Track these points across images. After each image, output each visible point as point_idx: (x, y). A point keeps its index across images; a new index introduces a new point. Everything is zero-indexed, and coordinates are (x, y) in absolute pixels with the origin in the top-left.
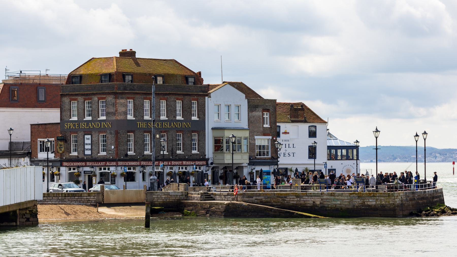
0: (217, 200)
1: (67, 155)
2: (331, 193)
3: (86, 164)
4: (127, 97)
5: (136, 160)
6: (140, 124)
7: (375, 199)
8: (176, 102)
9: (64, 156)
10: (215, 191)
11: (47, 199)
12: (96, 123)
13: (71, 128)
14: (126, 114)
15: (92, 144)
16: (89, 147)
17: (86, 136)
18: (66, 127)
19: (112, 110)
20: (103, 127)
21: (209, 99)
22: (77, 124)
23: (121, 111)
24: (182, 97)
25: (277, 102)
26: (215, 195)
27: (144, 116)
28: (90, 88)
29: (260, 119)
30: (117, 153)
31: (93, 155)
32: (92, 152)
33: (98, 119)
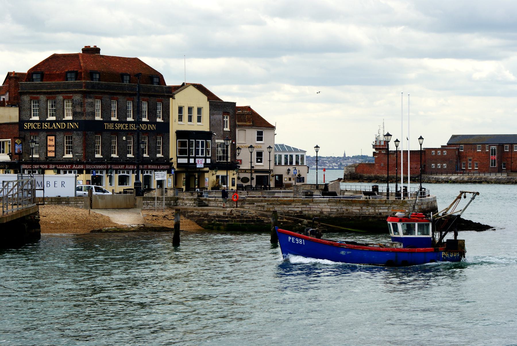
0: (211, 206)
1: (27, 157)
2: (339, 200)
3: (49, 167)
4: (95, 96)
5: (103, 164)
6: (107, 125)
7: (387, 206)
8: (142, 103)
9: (23, 158)
10: (207, 196)
11: (151, 203)
12: (61, 124)
13: (32, 128)
14: (93, 114)
15: (55, 146)
16: (53, 149)
17: (49, 137)
18: (26, 127)
19: (78, 110)
20: (69, 127)
21: (173, 100)
22: (39, 124)
23: (89, 111)
24: (148, 98)
25: (237, 105)
26: (209, 201)
27: (111, 116)
28: (54, 86)
29: (221, 122)
30: (85, 155)
31: (57, 157)
32: (56, 154)
33: (64, 119)
